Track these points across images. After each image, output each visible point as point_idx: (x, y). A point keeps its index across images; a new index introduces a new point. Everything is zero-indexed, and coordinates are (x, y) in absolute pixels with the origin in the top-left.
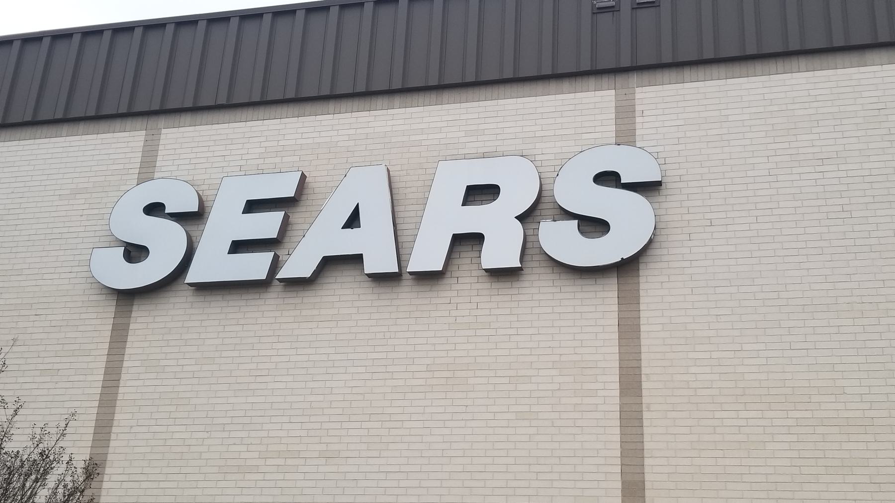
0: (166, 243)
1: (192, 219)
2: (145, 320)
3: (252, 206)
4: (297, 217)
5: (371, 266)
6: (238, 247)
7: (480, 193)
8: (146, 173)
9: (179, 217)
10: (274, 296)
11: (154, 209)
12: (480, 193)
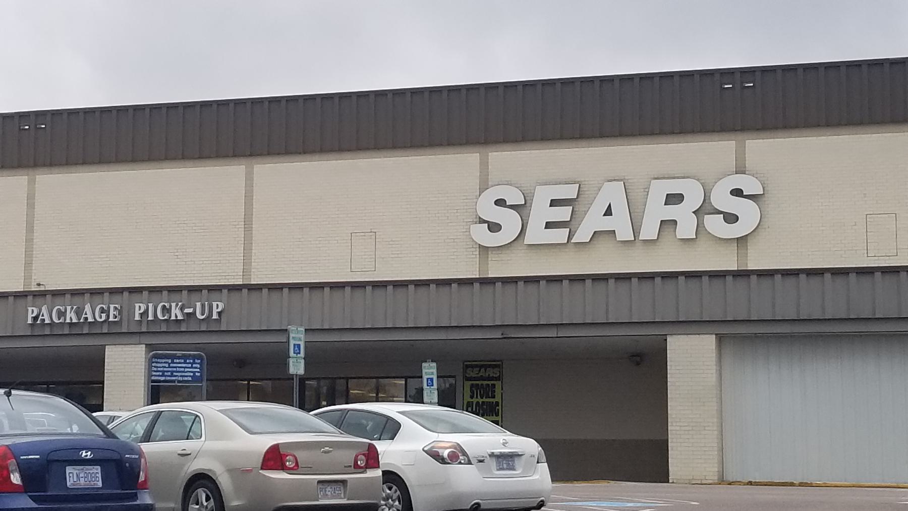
0: (510, 222)
3: (554, 203)
6: (549, 225)
7: (674, 199)
12: (674, 199)
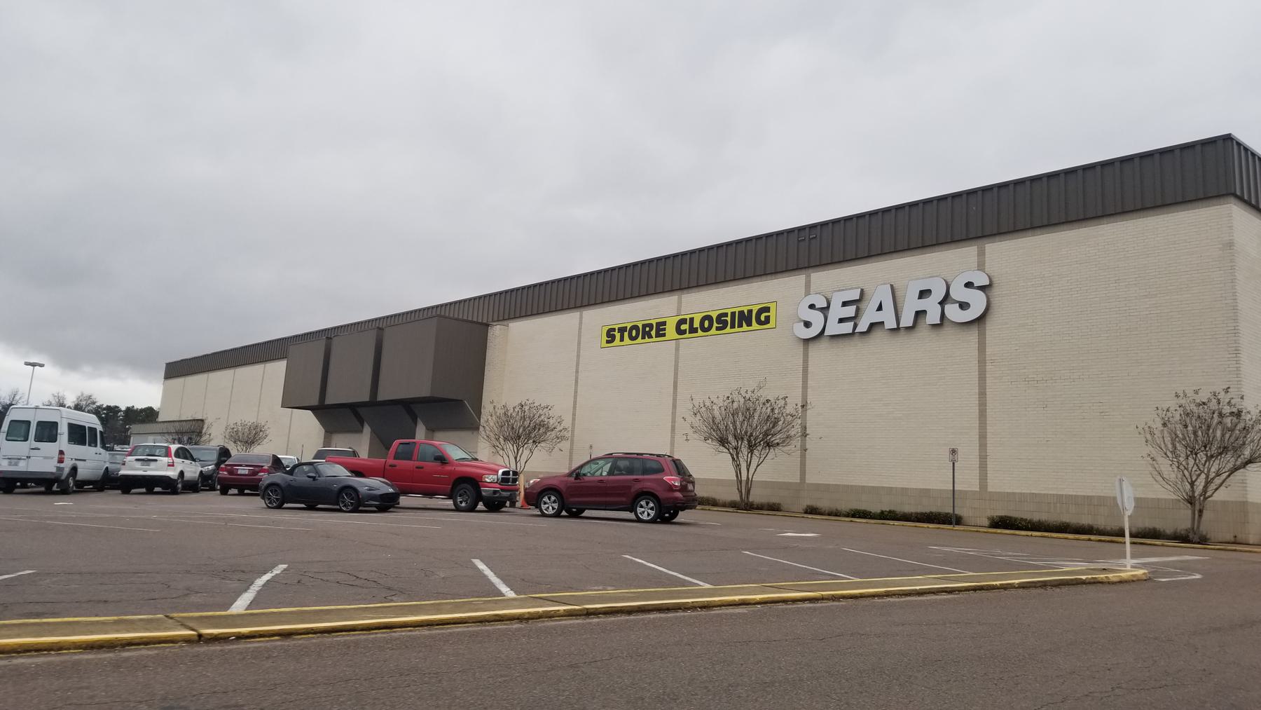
0: (817, 318)
1: (825, 310)
2: (816, 351)
3: (845, 304)
4: (862, 305)
5: (887, 326)
6: (841, 321)
7: (924, 294)
8: (808, 293)
9: (982, 288)
10: (856, 337)
11: (812, 307)
12: (924, 294)
